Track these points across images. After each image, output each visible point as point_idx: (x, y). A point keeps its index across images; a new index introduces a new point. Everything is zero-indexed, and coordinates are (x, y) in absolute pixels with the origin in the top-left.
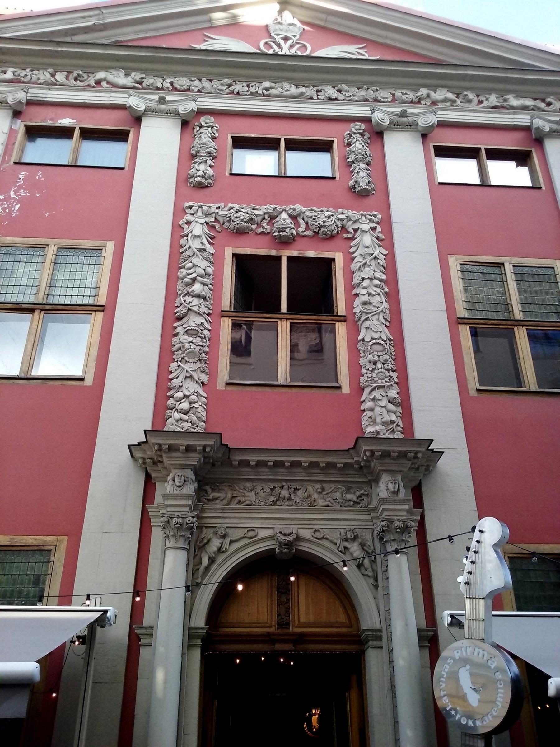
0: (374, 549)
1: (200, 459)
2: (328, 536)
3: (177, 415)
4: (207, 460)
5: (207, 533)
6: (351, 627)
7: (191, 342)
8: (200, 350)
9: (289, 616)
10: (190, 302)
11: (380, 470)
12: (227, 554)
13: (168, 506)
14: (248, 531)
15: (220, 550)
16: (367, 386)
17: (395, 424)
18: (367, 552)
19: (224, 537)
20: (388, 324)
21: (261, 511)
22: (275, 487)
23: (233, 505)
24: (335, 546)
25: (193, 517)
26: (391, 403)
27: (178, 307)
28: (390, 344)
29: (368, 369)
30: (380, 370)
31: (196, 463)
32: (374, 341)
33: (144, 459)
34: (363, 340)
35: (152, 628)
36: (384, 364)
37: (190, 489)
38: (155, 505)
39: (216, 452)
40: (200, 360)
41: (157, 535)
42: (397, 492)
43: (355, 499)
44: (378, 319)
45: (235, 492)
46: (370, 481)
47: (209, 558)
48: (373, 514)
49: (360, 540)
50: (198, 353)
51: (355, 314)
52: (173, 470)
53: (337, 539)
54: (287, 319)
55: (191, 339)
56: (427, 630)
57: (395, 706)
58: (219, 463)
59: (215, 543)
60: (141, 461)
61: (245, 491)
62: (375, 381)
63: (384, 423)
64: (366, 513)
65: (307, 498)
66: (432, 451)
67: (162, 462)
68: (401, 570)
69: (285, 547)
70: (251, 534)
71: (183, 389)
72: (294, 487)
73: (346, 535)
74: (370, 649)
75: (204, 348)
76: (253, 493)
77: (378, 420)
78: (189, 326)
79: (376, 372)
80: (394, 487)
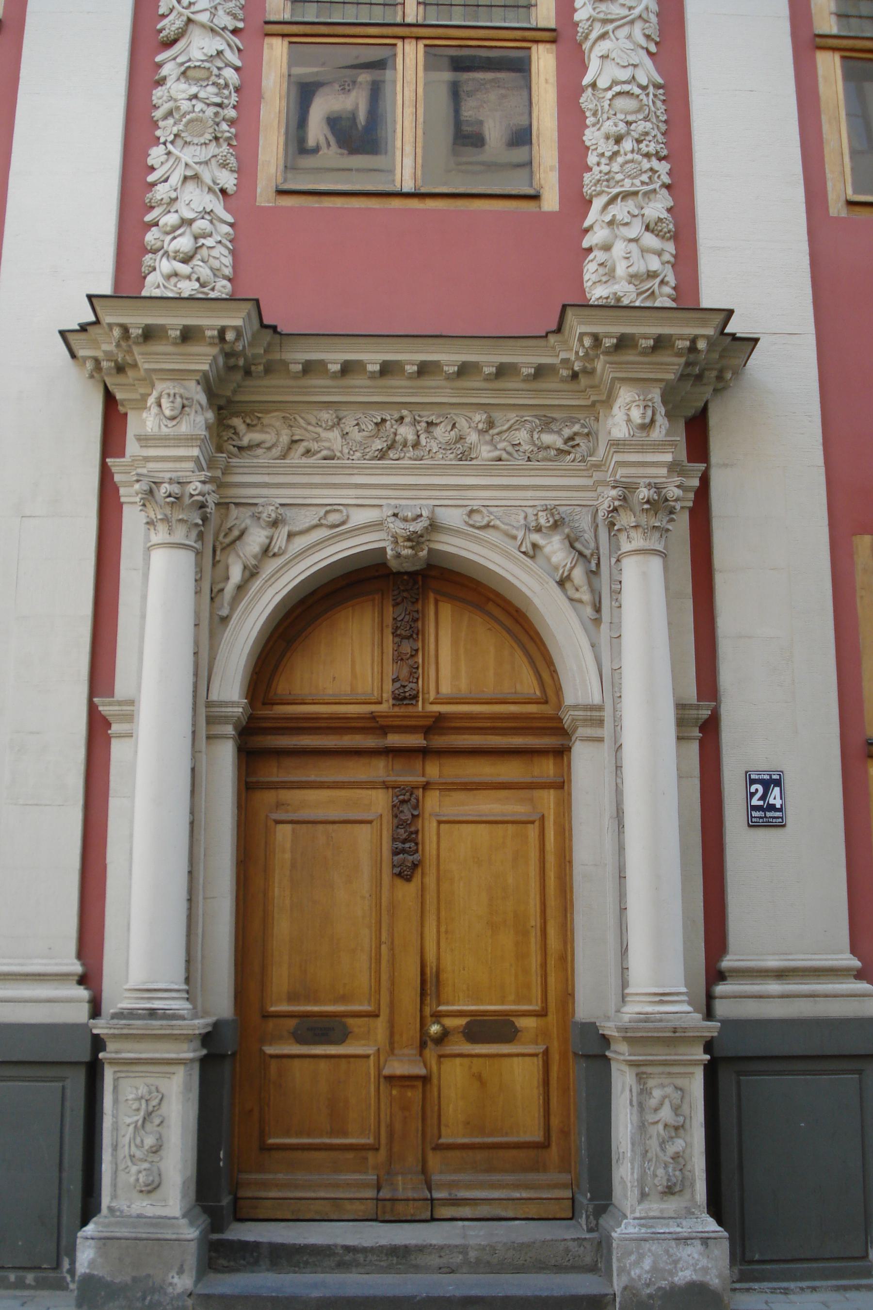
0: (598, 548)
1: (215, 358)
2: (498, 523)
3: (166, 266)
4: (232, 361)
5: (238, 517)
6: (546, 702)
7: (195, 96)
8: (216, 114)
9: (417, 682)
10: (190, 4)
11: (614, 379)
12: (280, 561)
13: (147, 459)
14: (327, 512)
15: (266, 551)
16: (601, 193)
17: (658, 280)
18: (581, 554)
19: (275, 524)
20: (653, 49)
21: (355, 471)
22: (384, 421)
23: (296, 458)
24: (512, 542)
25: (204, 482)
26: (652, 232)
27: (164, 16)
28: (655, 96)
29: (603, 154)
30: (630, 156)
31: (206, 367)
32: (617, 89)
33: (97, 361)
34: (594, 85)
35: (132, 702)
36: (639, 141)
37: (197, 422)
38: (127, 459)
39: (251, 344)
40: (216, 139)
41: (133, 520)
42: (648, 427)
43: (559, 444)
44: (629, 37)
45: (297, 431)
46: (594, 404)
47: (245, 567)
48: (597, 476)
49: (567, 530)
50: (211, 123)
51: (577, 24)
52: (157, 383)
53: (517, 529)
54: (418, 38)
55: (194, 90)
56: (698, 707)
57: (621, 849)
58: (261, 368)
59: (256, 539)
60: (90, 365)
61: (319, 430)
62: (618, 182)
63: (633, 278)
64: (585, 473)
65: (456, 442)
66: (733, 335)
67: (135, 366)
68: (644, 588)
69: (406, 544)
70: (333, 518)
71: (180, 205)
72: (425, 419)
73: (537, 519)
74: (578, 743)
75: (226, 111)
76: (335, 434)
77: (621, 270)
78: (190, 60)
79: (620, 160)
80: (644, 415)
